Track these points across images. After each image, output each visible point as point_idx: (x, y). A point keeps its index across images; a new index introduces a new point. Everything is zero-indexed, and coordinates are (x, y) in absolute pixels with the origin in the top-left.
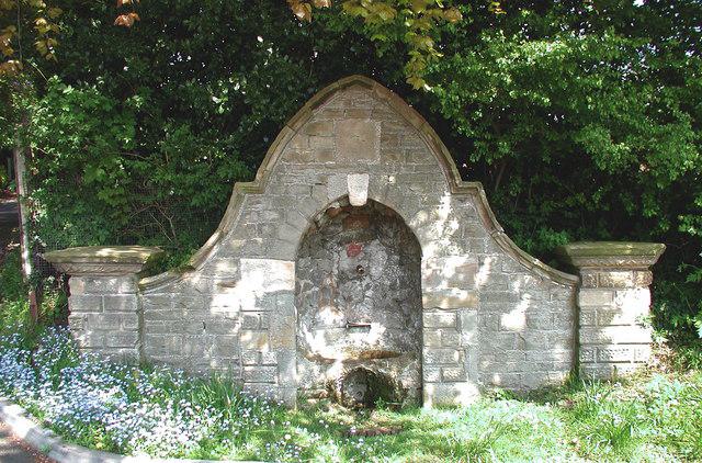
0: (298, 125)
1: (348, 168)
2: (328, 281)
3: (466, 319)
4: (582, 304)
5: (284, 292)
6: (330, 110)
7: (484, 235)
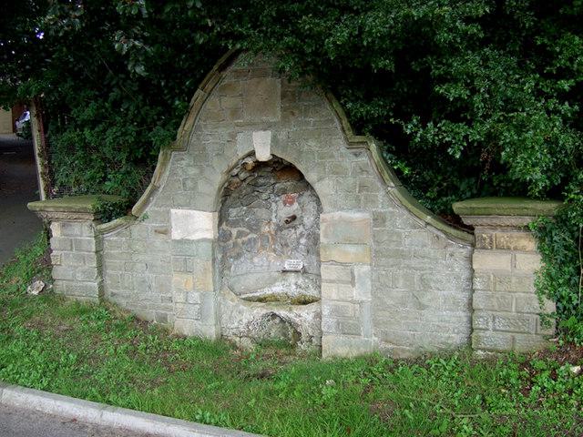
0: (209, 86)
1: (253, 126)
2: (266, 229)
3: (359, 275)
4: (474, 267)
5: (204, 240)
6: (236, 71)
7: (378, 190)
